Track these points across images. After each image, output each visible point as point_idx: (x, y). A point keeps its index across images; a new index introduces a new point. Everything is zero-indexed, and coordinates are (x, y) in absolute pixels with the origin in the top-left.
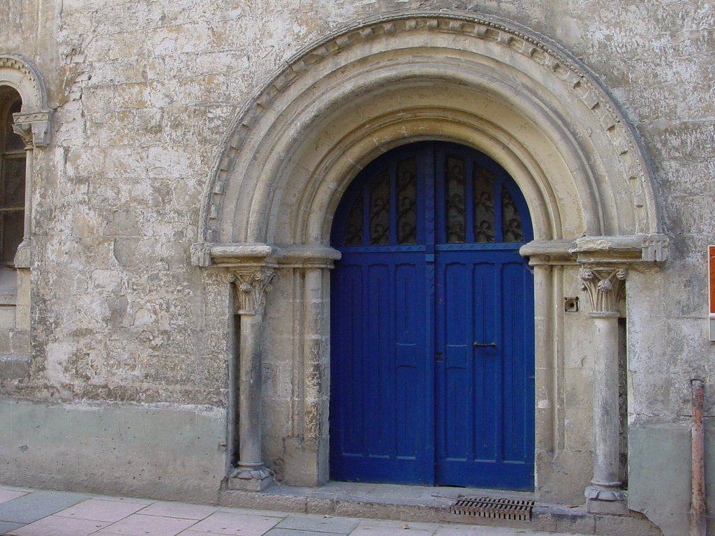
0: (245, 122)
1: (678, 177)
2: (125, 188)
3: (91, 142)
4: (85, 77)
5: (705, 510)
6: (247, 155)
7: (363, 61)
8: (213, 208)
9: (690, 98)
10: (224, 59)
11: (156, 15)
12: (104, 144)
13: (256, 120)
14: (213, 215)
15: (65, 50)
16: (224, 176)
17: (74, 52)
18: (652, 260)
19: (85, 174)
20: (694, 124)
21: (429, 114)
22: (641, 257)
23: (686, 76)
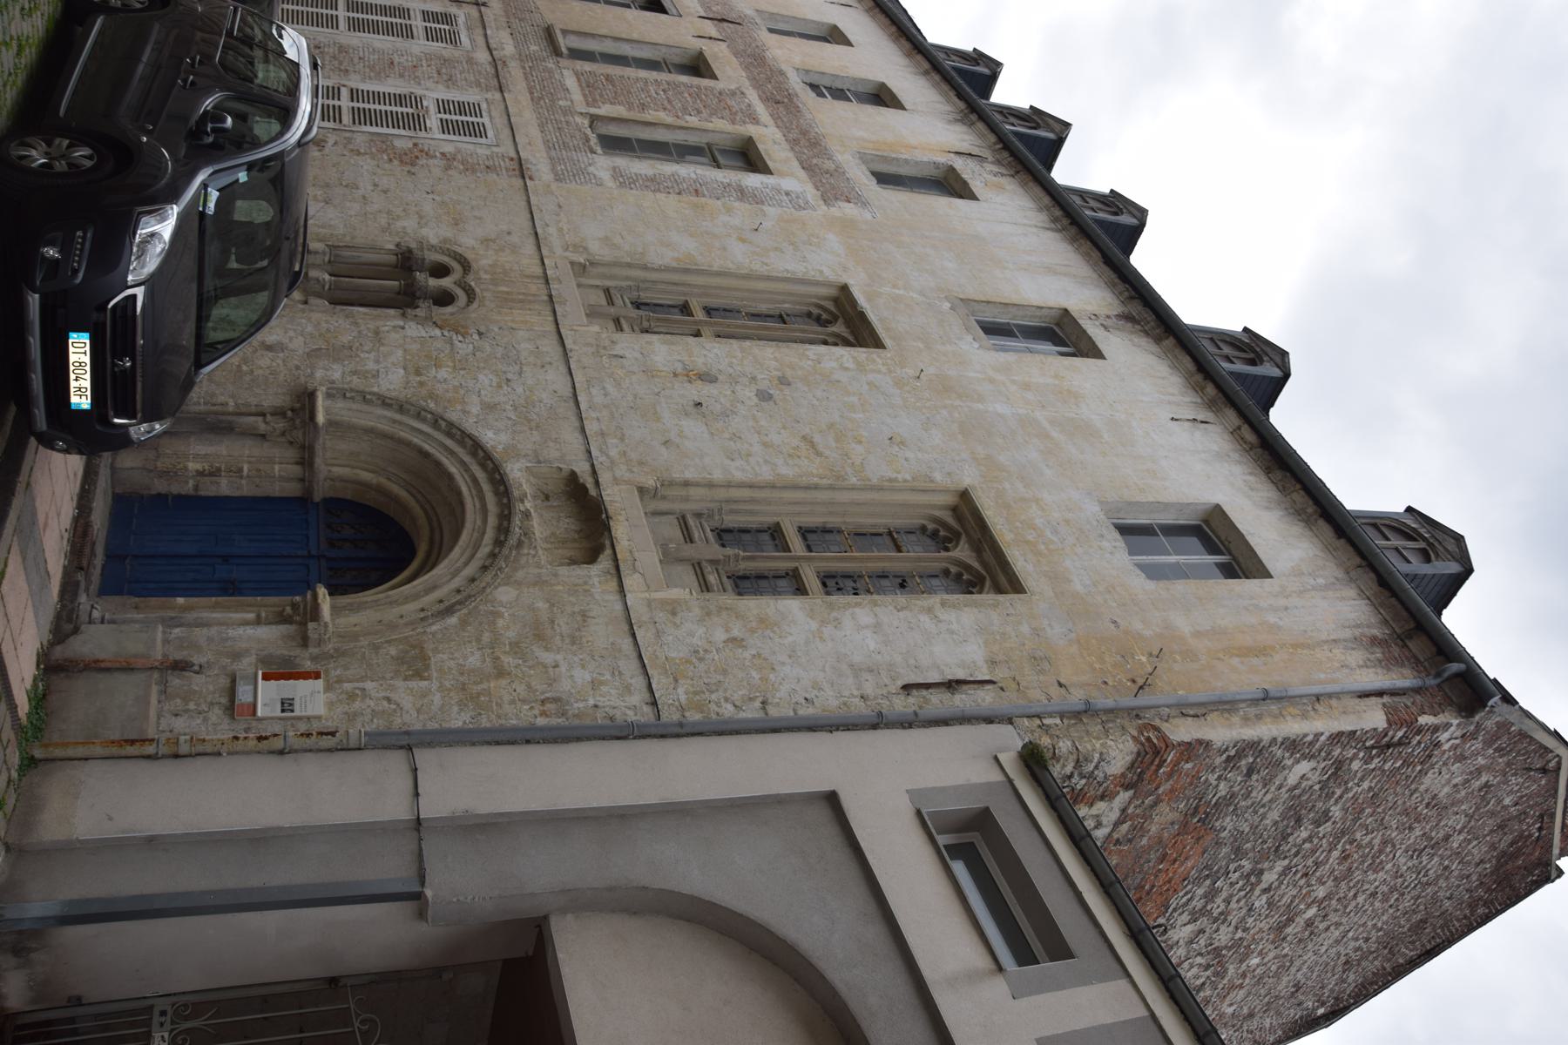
0: (423, 413)
1: (781, 684)
2: (372, 356)
3: (408, 340)
4: (460, 338)
5: (2, 599)
6: (398, 417)
7: (475, 480)
8: (353, 394)
9: (452, 662)
10: (475, 410)
11: (510, 376)
12: (407, 346)
13: (424, 420)
14: (348, 395)
15: (482, 329)
16: (380, 402)
17: (480, 334)
18: (292, 489)
19: (382, 335)
20: (429, 665)
21: (660, 286)
22: (292, 711)
23: (471, 659)
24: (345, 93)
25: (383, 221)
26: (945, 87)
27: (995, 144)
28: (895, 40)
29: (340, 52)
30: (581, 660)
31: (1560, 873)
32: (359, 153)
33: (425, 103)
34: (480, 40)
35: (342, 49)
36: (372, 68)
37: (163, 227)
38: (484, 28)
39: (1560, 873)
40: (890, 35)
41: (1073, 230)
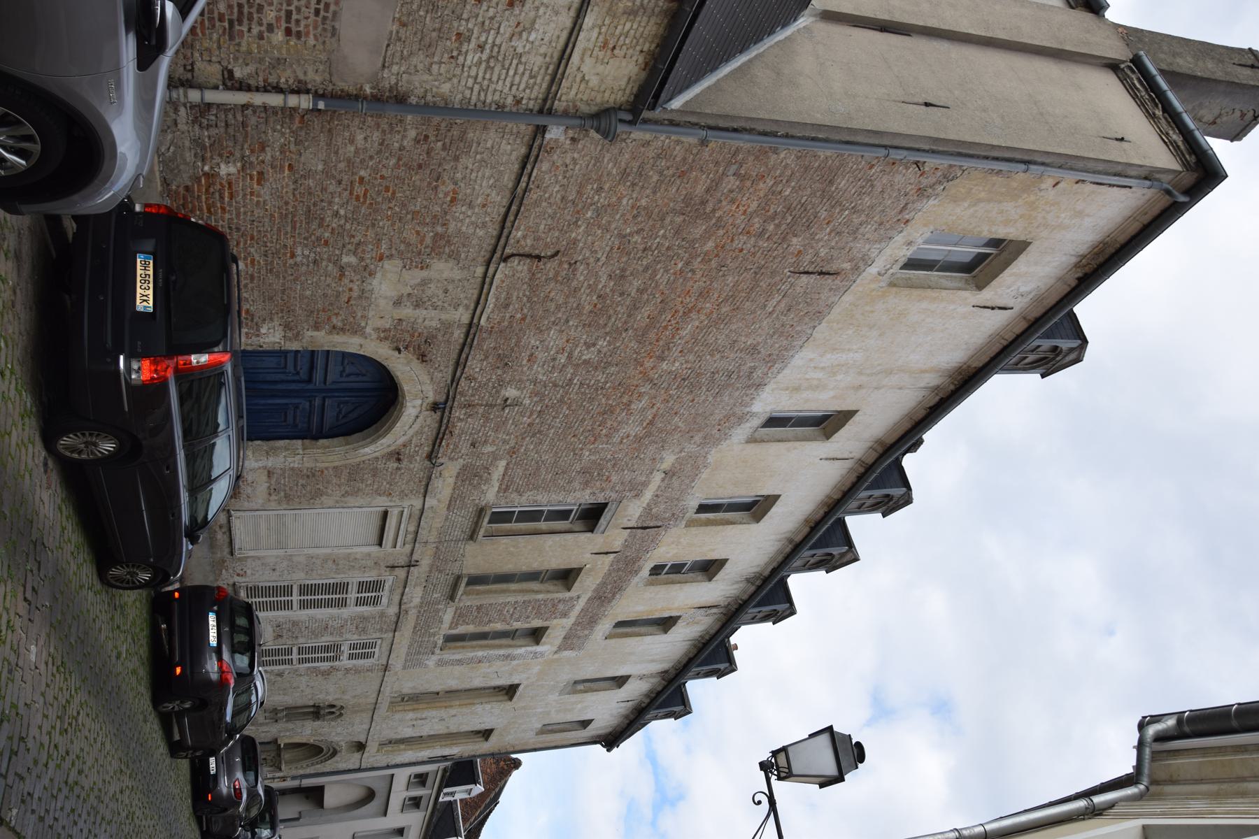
24: (295, 650)
25: (310, 697)
26: (780, 558)
27: (741, 600)
28: (823, 503)
29: (293, 626)
30: (252, 151)
31: (850, 556)
32: (301, 675)
33: (342, 649)
34: (396, 598)
35: (295, 624)
36: (313, 633)
37: (238, 736)
38: (405, 587)
39: (850, 556)
40: (828, 497)
41: (701, 645)
